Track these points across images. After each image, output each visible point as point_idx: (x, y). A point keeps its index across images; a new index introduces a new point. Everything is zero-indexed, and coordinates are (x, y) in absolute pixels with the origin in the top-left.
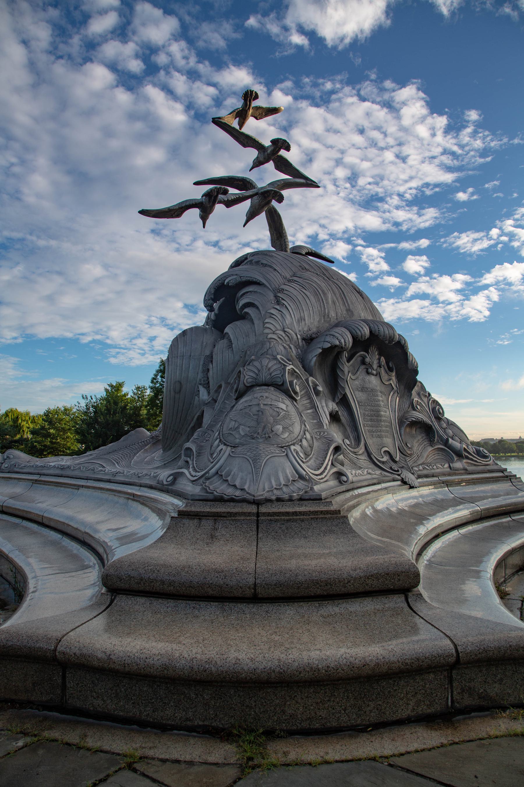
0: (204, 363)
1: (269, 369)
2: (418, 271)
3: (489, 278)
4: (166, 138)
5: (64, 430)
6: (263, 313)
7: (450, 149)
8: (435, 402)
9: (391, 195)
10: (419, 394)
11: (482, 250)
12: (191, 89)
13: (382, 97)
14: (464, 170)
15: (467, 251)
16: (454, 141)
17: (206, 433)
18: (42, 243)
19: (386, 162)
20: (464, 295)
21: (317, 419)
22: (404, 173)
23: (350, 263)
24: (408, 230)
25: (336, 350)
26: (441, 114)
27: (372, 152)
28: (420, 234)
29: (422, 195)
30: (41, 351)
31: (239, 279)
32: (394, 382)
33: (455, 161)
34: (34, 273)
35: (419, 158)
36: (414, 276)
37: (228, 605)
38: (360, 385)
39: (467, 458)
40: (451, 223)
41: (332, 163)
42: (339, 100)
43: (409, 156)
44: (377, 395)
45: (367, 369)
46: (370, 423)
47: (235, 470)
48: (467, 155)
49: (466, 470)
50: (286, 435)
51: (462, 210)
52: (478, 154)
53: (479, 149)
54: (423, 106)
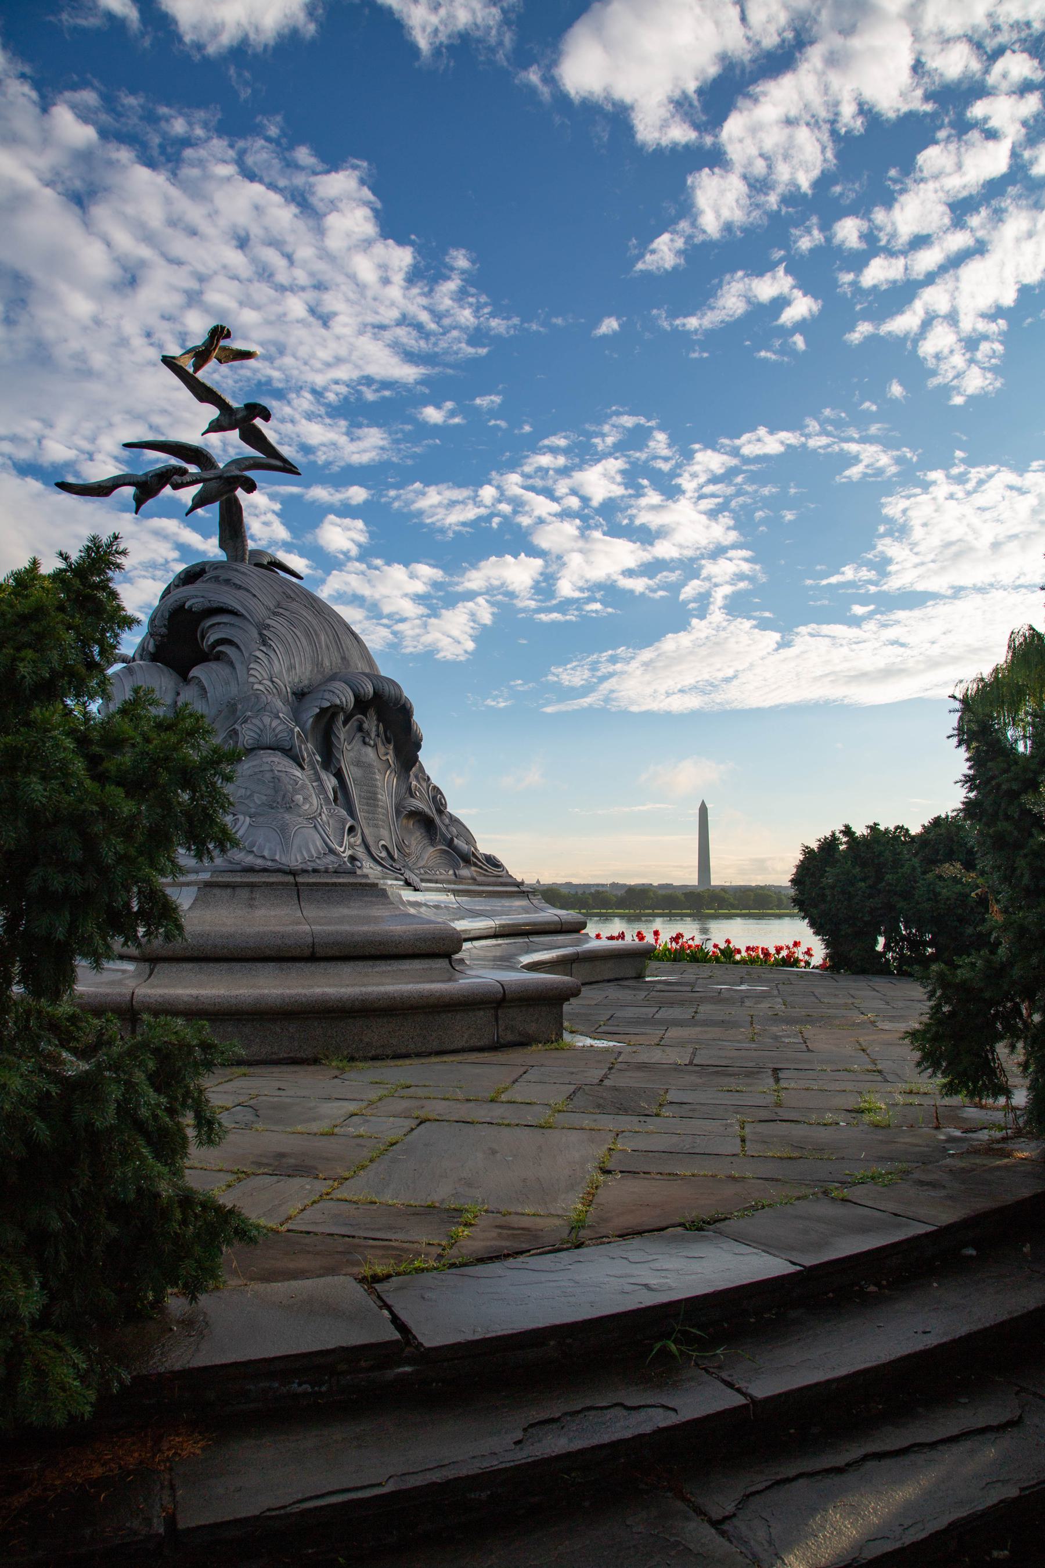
1: (274, 730)
2: (345, 549)
3: (474, 580)
6: (246, 655)
7: (414, 317)
8: (436, 789)
9: (299, 389)
10: (417, 777)
11: (464, 524)
13: (290, 179)
14: (437, 365)
15: (438, 521)
19: (288, 318)
20: (428, 606)
22: (326, 347)
23: (208, 515)
24: (328, 464)
25: (332, 710)
26: (401, 242)
27: (262, 291)
28: (350, 475)
31: (207, 605)
32: (391, 758)
36: (336, 557)
37: (285, 965)
39: (475, 865)
40: (410, 462)
41: (178, 299)
44: (374, 773)
47: (260, 841)
48: (444, 334)
49: (475, 879)
50: (307, 807)
51: (431, 442)
52: (465, 336)
53: (468, 328)
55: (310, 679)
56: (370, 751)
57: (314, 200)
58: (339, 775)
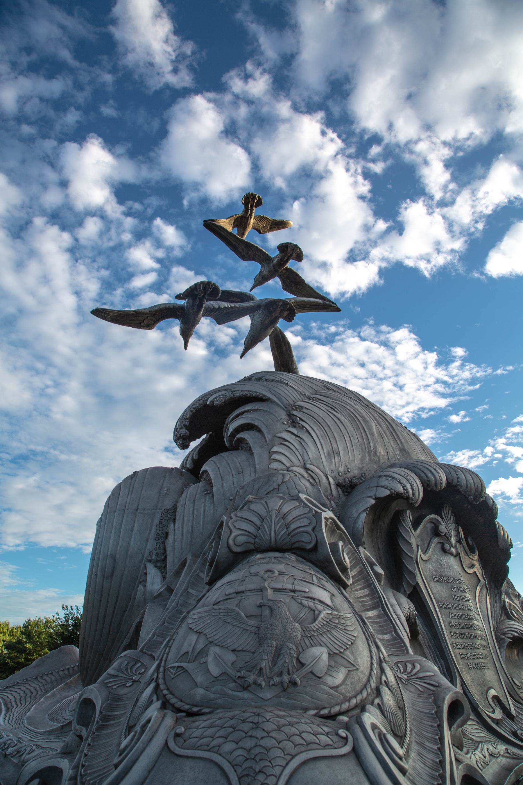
0: (160, 523)
1: (284, 517)
4: (188, 368)
5: (41, 645)
6: (268, 437)
12: (213, 330)
13: (379, 338)
16: (444, 373)
17: (137, 661)
18: (63, 457)
19: (384, 390)
21: (390, 633)
22: (402, 399)
26: (431, 351)
27: (373, 382)
29: (418, 418)
30: (42, 559)
32: (478, 569)
33: (447, 389)
34: (48, 483)
35: (416, 386)
38: (436, 571)
40: (446, 442)
42: (342, 340)
43: (405, 385)
44: (463, 591)
45: (443, 545)
46: (460, 641)
51: (456, 431)
53: (468, 379)
54: (416, 345)
55: (361, 469)
56: (453, 562)
57: (390, 344)
58: (416, 596)
